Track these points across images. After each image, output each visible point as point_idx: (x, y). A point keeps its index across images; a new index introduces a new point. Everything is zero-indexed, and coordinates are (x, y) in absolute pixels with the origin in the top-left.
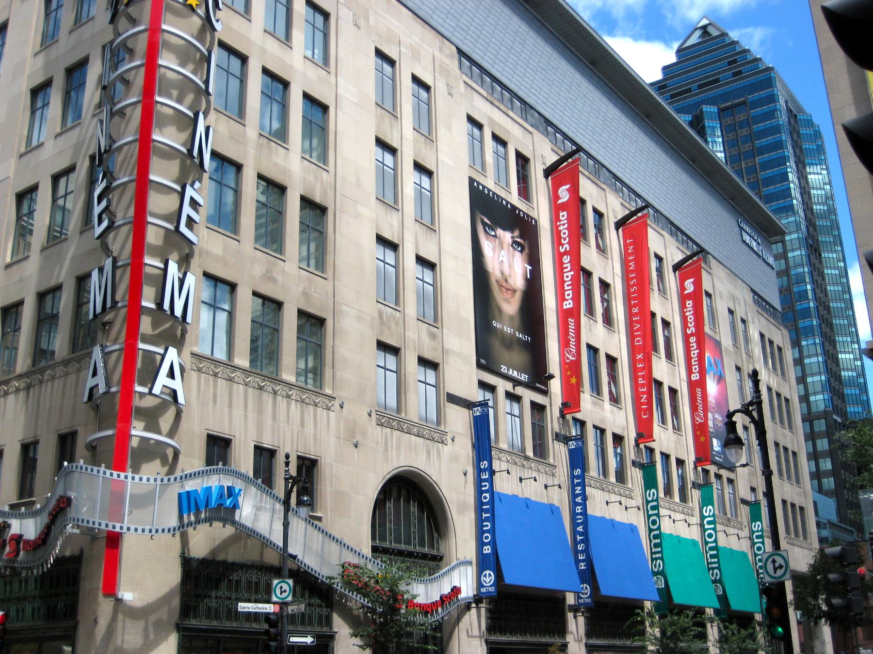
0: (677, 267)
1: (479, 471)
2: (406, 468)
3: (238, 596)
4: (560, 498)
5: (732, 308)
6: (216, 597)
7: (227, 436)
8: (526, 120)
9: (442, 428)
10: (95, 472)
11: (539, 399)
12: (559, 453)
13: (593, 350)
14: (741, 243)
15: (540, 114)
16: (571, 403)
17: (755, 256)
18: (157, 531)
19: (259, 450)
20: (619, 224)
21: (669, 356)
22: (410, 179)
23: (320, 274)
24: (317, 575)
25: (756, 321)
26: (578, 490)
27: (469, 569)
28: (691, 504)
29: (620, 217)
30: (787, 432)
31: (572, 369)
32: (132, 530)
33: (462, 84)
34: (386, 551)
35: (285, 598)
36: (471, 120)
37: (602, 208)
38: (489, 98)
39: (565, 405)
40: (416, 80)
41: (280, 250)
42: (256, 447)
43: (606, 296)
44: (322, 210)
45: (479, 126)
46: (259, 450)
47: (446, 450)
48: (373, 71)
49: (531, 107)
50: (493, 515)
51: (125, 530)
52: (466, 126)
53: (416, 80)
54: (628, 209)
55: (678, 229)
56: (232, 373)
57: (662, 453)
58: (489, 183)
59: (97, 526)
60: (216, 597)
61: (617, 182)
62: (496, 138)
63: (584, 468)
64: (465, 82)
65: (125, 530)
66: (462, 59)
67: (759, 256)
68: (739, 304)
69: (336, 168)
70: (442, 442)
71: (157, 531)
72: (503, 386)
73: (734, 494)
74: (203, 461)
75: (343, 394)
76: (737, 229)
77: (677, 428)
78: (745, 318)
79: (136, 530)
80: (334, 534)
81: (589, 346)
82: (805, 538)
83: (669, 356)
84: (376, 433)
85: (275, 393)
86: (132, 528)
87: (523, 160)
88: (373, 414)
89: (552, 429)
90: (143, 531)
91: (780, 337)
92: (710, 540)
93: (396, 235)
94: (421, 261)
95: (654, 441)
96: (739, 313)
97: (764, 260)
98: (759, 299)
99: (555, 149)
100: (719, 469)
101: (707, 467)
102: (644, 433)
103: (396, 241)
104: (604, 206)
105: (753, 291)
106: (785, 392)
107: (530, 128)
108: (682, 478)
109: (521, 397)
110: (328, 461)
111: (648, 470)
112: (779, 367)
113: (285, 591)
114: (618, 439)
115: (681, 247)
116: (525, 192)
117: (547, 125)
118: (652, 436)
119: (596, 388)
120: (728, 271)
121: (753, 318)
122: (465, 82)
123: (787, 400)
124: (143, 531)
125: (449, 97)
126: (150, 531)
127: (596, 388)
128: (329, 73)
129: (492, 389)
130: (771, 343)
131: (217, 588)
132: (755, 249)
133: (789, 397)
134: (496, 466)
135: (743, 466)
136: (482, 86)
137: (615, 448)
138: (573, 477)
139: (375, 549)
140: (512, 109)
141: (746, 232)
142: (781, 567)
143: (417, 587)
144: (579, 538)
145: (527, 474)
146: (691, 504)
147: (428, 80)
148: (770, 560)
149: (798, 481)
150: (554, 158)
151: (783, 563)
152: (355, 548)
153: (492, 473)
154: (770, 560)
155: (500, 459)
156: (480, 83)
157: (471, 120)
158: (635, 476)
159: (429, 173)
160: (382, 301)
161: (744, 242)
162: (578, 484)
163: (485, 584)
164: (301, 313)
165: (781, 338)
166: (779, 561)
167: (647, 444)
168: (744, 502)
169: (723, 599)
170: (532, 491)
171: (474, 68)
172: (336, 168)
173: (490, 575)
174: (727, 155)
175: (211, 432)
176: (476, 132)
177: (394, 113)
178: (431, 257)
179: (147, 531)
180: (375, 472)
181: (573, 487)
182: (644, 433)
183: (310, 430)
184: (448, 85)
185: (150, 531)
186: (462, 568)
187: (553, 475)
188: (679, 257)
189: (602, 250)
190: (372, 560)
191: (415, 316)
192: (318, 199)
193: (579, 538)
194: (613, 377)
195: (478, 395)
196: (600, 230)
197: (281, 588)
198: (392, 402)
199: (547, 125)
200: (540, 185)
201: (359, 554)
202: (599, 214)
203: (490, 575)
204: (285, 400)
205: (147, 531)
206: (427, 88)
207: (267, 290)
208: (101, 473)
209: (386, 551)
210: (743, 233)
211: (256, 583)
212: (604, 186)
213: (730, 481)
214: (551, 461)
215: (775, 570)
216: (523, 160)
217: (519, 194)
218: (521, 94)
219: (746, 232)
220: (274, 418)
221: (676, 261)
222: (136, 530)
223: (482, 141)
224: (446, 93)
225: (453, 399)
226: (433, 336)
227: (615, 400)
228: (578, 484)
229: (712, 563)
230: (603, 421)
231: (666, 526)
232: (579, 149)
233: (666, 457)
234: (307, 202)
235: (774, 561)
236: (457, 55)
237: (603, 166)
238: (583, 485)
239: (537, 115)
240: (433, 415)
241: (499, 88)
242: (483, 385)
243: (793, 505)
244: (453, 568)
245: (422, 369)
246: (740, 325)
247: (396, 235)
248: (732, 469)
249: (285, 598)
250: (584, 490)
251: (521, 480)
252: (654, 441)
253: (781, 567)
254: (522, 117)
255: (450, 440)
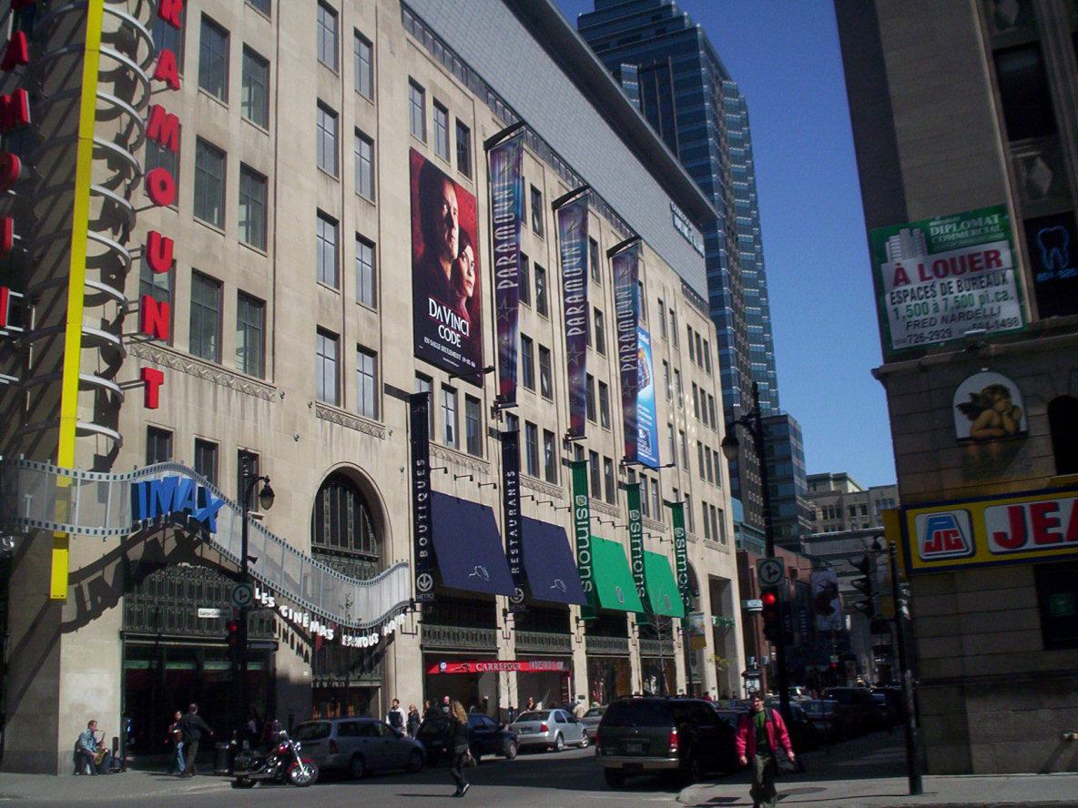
0: (611, 253)
1: (415, 468)
2: (355, 467)
3: (140, 598)
4: (491, 498)
5: (662, 299)
6: (179, 605)
7: (168, 429)
8: (467, 85)
9: (379, 422)
10: (39, 468)
11: (475, 392)
12: (494, 448)
13: (527, 340)
14: (673, 229)
15: (481, 78)
16: (508, 396)
17: (685, 242)
18: (110, 532)
19: (242, 454)
20: (556, 205)
21: (601, 349)
22: (350, 144)
23: (261, 251)
24: (259, 578)
25: (684, 312)
26: (511, 492)
27: (406, 570)
28: (617, 505)
29: (557, 197)
30: (710, 430)
31: (507, 363)
32: (84, 532)
33: (405, 40)
34: (323, 551)
35: (246, 603)
36: (412, 82)
37: (539, 187)
38: (431, 58)
39: (500, 399)
40: (358, 34)
41: (595, 421)
42: (197, 440)
43: (540, 282)
44: (262, 179)
45: (421, 90)
46: (242, 454)
47: (385, 443)
48: (316, 23)
49: (473, 70)
50: (429, 517)
51: (76, 531)
52: (409, 88)
53: (358, 34)
54: (567, 190)
55: (613, 210)
56: (173, 359)
57: (527, 423)
58: (430, 154)
59: (43, 526)
60: (139, 601)
61: (553, 157)
62: (437, 104)
63: (517, 468)
64: (408, 40)
65: (76, 531)
66: (405, 12)
67: (688, 241)
68: (669, 295)
69: (276, 132)
70: (380, 437)
71: (110, 532)
72: (439, 376)
73: (657, 494)
74: (143, 459)
75: (283, 382)
76: (669, 214)
77: (606, 425)
78: (673, 309)
79: (88, 531)
80: (277, 535)
81: (523, 336)
82: (723, 541)
83: (601, 349)
84: (315, 425)
85: (216, 381)
86: (84, 529)
87: (463, 129)
88: (313, 406)
89: (486, 424)
90: (96, 532)
91: (707, 330)
92: (583, 562)
93: (336, 210)
94: (361, 239)
95: (517, 406)
96: (669, 305)
97: (696, 249)
98: (688, 290)
99: (496, 119)
100: (450, 378)
101: (632, 467)
102: (577, 430)
103: (336, 217)
104: (542, 185)
105: (682, 280)
106: (709, 390)
107: (471, 94)
108: (609, 478)
109: (222, 283)
110: (268, 456)
111: (578, 467)
112: (704, 362)
113: (245, 596)
114: (549, 435)
115: (614, 231)
116: (465, 165)
117: (486, 91)
118: (514, 400)
119: (529, 383)
120: (659, 258)
121: (681, 310)
122: (408, 40)
123: (710, 397)
124: (96, 532)
125: (391, 55)
126: (103, 532)
127: (529, 383)
128: (270, 22)
129: (429, 379)
130: (698, 336)
131: (139, 592)
132: (686, 235)
133: (712, 395)
134: (432, 465)
135: (669, 466)
136: (424, 44)
137: (545, 444)
138: (506, 479)
139: (314, 550)
140: (453, 71)
141: (678, 217)
142: (776, 573)
143: (359, 590)
144: (512, 543)
145: (461, 471)
146: (617, 505)
147: (371, 37)
148: (765, 566)
149: (718, 484)
150: (496, 130)
151: (778, 569)
152: (294, 547)
153: (428, 470)
154: (765, 566)
155: (435, 455)
156: (422, 41)
157: (412, 82)
158: (566, 474)
159: (369, 141)
160: (322, 283)
161: (676, 227)
162: (512, 487)
163: (422, 590)
164: (196, 273)
165: (707, 330)
166: (774, 567)
167: (577, 442)
168: (666, 503)
169: (646, 600)
170: (465, 491)
171: (416, 23)
172: (276, 132)
173: (427, 579)
174: (644, 102)
175: (152, 424)
176: (418, 96)
177: (336, 68)
178: (373, 237)
179: (99, 533)
180: (315, 468)
181: (506, 488)
182: (577, 430)
183: (249, 423)
184: (390, 41)
185: (103, 532)
186: (401, 569)
187: (486, 472)
188: (613, 243)
189: (539, 232)
190: (312, 560)
191: (354, 298)
192: (257, 167)
193: (512, 543)
194: (546, 371)
195: (413, 387)
196: (537, 212)
197: (241, 592)
198: (331, 392)
199: (486, 91)
200: (479, 157)
201: (302, 556)
202: (535, 192)
203: (427, 579)
204: (226, 388)
205: (99, 533)
206: (369, 44)
207: (205, 268)
208: (47, 470)
209: (323, 551)
210: (677, 219)
211: (179, 586)
212: (542, 162)
213: (654, 481)
214: (485, 458)
215: (770, 575)
216: (463, 129)
217: (459, 169)
218: (462, 55)
219: (678, 217)
220: (215, 409)
221: (610, 247)
222: (88, 531)
223: (423, 107)
224: (389, 51)
225: (390, 390)
226: (371, 322)
227: (547, 394)
228: (512, 487)
229: (584, 526)
230: (534, 416)
231: (596, 530)
232: (523, 122)
233: (594, 454)
234: (246, 170)
235: (769, 568)
236: (400, 8)
237: (542, 139)
238: (516, 487)
239: (478, 79)
240: (370, 408)
241: (441, 48)
242: (420, 375)
243: (712, 507)
244: (393, 570)
245: (321, 337)
246: (669, 316)
247: (336, 210)
248: (656, 469)
249: (246, 603)
250: (518, 492)
251: (455, 477)
252: (517, 406)
253: (776, 573)
254: (462, 81)
255: (387, 435)
